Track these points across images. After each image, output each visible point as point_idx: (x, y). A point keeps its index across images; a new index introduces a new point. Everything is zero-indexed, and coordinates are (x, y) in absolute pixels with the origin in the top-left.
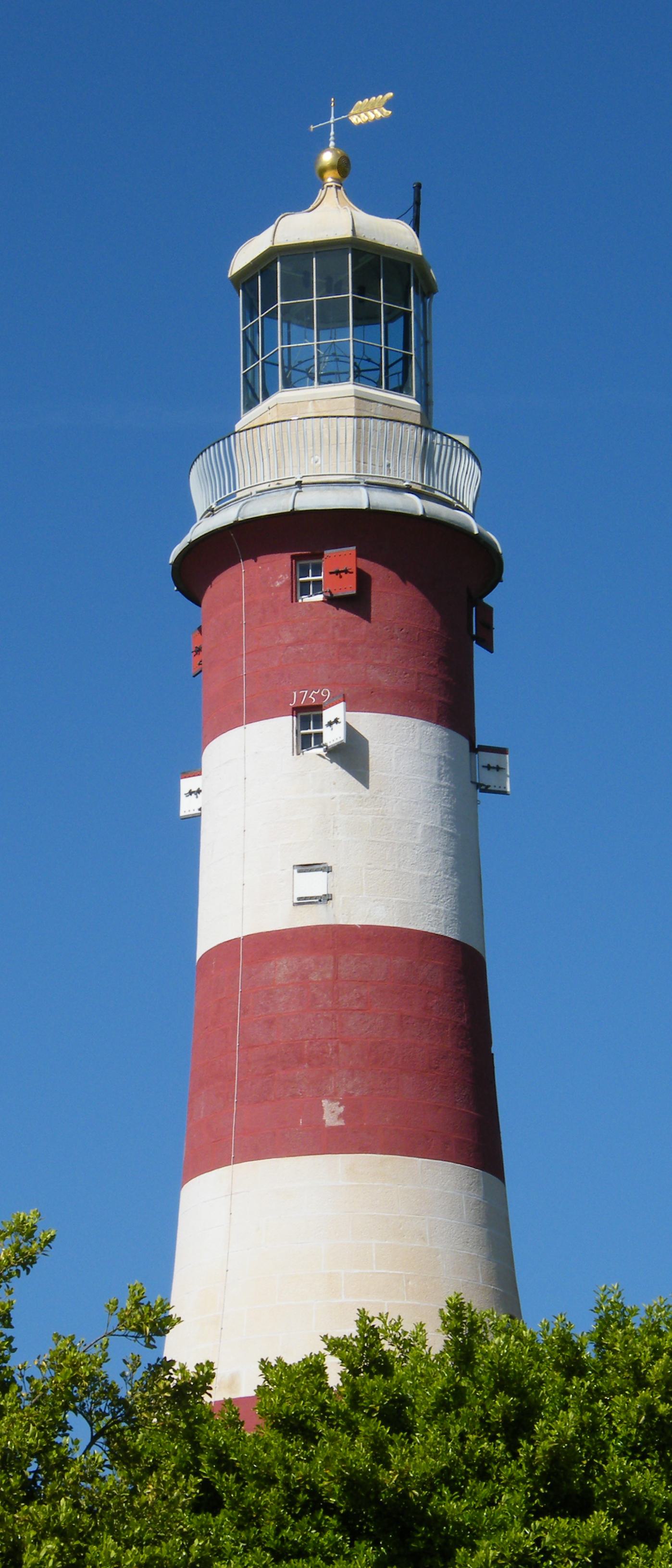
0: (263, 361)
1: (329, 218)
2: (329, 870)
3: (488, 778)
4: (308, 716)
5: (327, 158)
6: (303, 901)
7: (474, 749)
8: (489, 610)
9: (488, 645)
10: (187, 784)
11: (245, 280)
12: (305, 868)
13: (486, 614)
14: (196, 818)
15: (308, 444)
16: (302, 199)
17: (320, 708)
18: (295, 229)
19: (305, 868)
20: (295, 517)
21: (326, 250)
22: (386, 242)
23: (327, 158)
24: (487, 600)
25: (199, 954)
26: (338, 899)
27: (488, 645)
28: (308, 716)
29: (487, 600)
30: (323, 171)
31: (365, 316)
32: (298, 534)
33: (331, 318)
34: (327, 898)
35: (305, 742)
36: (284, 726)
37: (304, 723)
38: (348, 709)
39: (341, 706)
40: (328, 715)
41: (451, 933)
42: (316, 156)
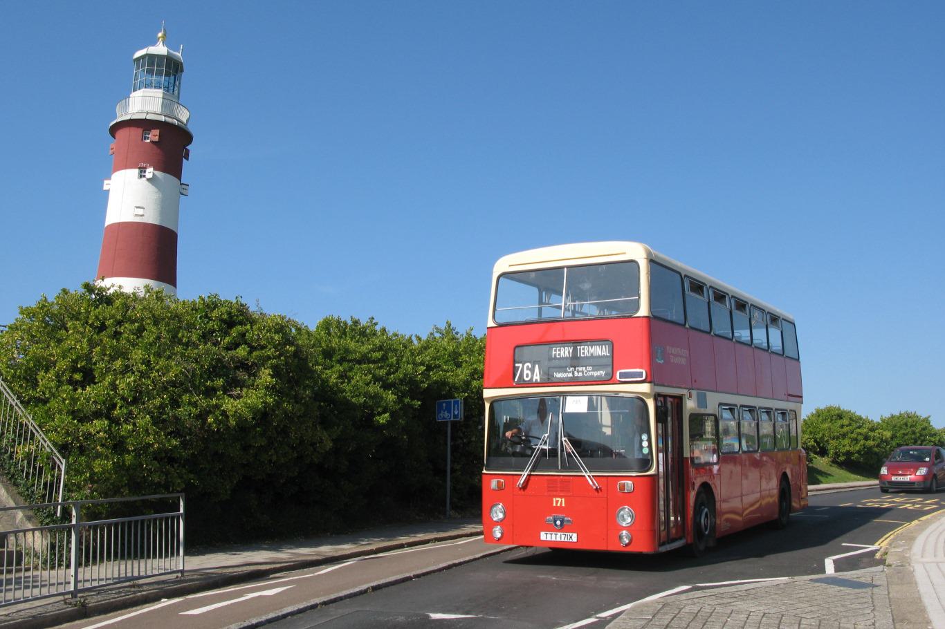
0: (140, 82)
1: (160, 49)
3: (184, 192)
4: (142, 171)
5: (160, 35)
6: (136, 215)
7: (181, 184)
8: (189, 151)
9: (187, 159)
10: (106, 182)
11: (138, 59)
12: (138, 207)
13: (188, 151)
14: (109, 191)
15: (145, 102)
16: (154, 43)
17: (146, 168)
18: (153, 50)
19: (138, 207)
20: (146, 120)
21: (160, 57)
22: (701, 277)
23: (160, 35)
24: (188, 147)
25: (106, 225)
26: (146, 216)
27: (187, 159)
28: (142, 171)
29: (188, 147)
30: (159, 39)
31: (167, 74)
32: (144, 125)
33: (159, 73)
36: (136, 171)
37: (141, 172)
38: (154, 169)
41: (156, 222)
42: (157, 34)
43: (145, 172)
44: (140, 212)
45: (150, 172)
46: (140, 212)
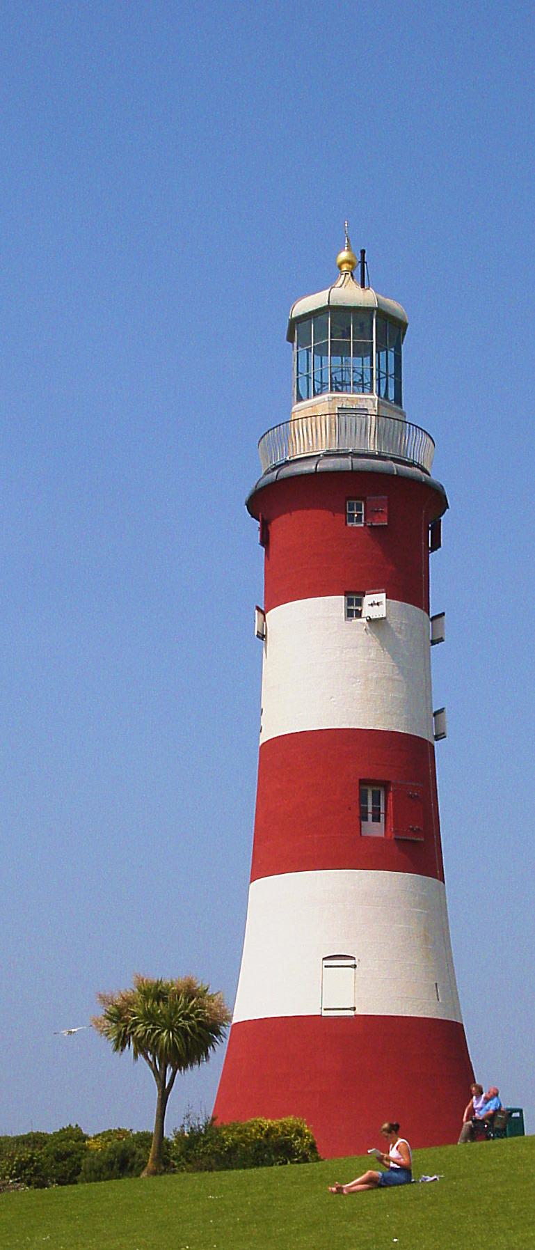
1: (348, 293)
5: (344, 255)
16: (330, 284)
35: (350, 614)
36: (341, 600)
37: (350, 602)
39: (381, 597)
40: (368, 599)
43: (360, 603)
45: (376, 604)
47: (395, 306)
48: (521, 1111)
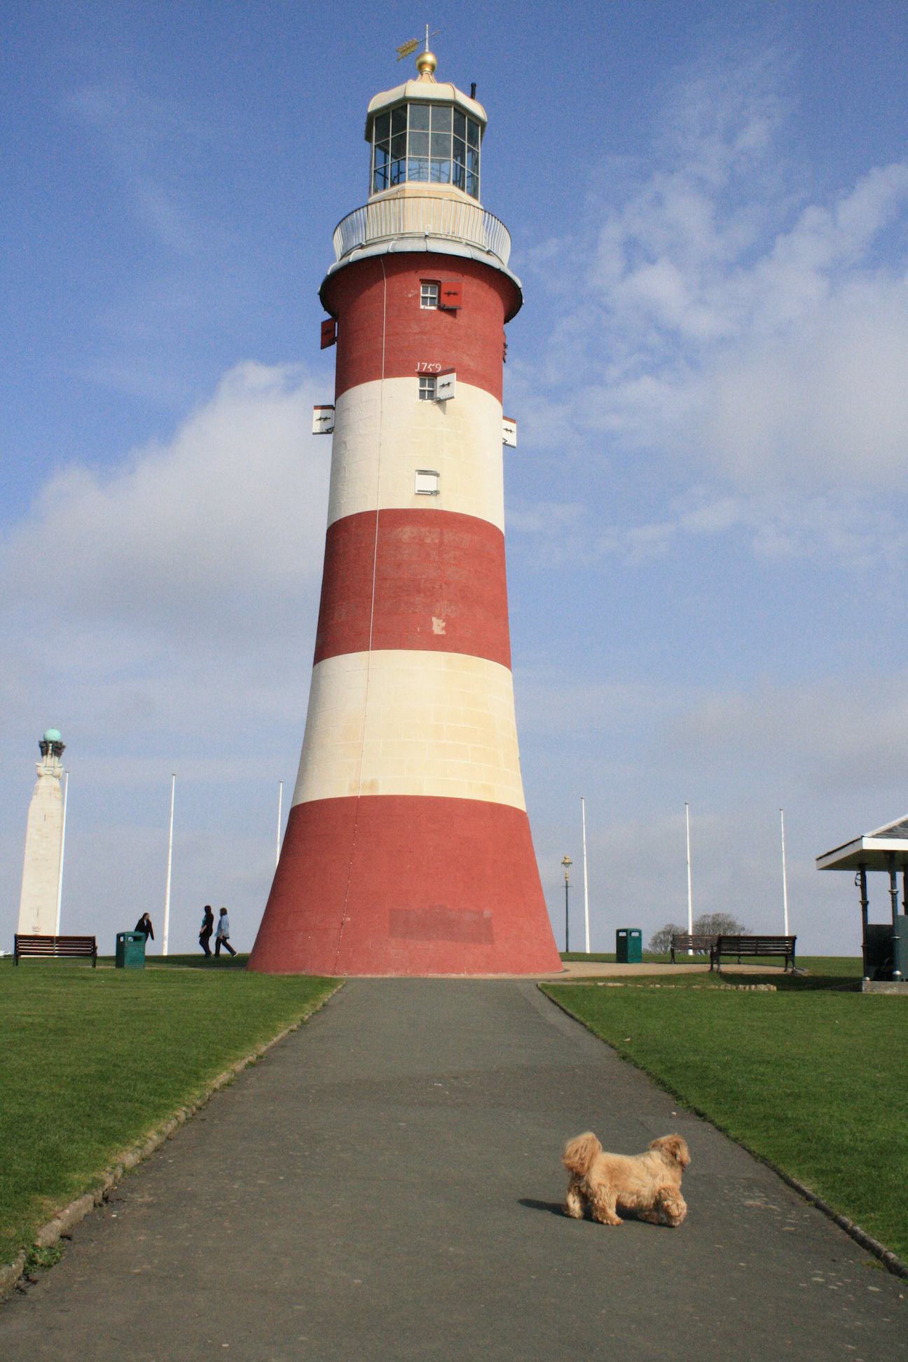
2: (437, 475)
4: (429, 377)
6: (421, 493)
12: (528, 1203)
19: (528, 1203)
34: (436, 493)
36: (412, 384)
40: (441, 380)
44: (428, 483)
46: (428, 483)
47: (502, 259)
48: (640, 932)
